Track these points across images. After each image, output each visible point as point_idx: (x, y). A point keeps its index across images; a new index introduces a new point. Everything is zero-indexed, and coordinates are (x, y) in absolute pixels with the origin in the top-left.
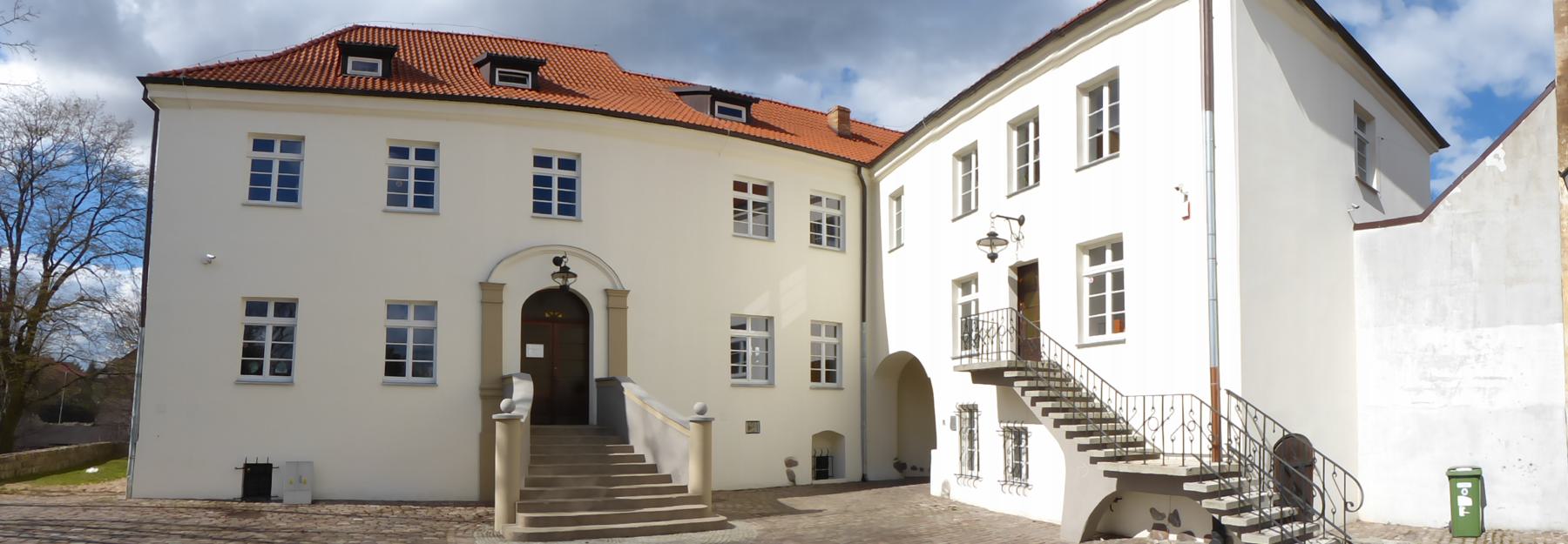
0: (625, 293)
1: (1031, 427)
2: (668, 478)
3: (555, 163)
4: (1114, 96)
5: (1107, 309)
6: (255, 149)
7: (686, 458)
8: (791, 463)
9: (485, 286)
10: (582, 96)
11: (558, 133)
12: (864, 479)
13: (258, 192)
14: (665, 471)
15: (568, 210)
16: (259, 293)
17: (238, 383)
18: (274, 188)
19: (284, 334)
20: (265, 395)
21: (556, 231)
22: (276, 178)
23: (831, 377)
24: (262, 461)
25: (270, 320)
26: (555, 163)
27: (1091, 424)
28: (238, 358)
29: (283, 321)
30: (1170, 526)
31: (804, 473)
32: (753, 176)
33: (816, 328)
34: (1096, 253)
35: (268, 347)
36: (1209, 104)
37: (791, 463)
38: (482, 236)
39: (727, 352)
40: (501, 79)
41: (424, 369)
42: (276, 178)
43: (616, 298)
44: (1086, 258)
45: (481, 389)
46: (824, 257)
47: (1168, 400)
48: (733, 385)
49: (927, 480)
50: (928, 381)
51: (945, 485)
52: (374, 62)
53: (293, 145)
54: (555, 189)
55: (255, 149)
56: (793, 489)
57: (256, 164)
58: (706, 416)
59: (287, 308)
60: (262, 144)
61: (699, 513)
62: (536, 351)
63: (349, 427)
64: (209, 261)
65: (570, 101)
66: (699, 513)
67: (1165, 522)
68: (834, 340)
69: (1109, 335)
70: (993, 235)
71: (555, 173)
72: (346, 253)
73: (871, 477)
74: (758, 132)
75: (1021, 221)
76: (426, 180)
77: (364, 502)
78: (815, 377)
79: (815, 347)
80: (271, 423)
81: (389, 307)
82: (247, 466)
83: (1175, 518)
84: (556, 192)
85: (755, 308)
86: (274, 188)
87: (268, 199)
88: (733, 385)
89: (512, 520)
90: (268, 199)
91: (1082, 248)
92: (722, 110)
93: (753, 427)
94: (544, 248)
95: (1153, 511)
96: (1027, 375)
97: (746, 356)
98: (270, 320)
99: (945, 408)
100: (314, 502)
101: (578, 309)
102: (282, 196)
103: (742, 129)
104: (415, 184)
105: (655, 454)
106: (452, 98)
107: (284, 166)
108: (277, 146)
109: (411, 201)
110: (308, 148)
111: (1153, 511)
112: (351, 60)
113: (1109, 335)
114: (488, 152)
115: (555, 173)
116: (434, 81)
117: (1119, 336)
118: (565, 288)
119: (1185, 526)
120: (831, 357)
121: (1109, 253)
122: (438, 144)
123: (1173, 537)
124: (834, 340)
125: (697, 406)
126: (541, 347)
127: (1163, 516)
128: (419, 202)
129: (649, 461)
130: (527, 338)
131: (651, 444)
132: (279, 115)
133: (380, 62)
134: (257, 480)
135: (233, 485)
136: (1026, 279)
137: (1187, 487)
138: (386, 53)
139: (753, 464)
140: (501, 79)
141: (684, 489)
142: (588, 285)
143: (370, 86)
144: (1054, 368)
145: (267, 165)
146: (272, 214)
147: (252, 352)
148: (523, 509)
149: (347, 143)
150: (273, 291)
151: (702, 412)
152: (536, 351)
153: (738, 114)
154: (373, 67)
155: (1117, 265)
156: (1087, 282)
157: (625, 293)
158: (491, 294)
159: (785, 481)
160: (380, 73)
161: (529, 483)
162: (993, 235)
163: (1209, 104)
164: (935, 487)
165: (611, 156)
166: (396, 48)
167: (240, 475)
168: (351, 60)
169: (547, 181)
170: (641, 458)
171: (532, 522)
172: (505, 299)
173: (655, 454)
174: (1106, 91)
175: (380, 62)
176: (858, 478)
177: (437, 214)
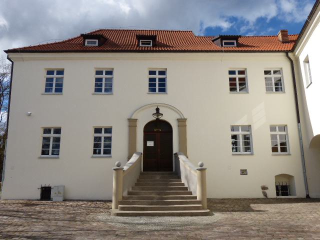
0: (185, 120)
3: (237, 73)
6: (47, 74)
8: (264, 188)
9: (130, 120)
10: (251, 46)
11: (157, 61)
12: (308, 196)
13: (48, 89)
15: (163, 89)
16: (48, 126)
17: (92, 157)
18: (157, 88)
19: (57, 140)
20: (49, 162)
21: (158, 98)
22: (54, 84)
23: (284, 149)
24: (47, 186)
25: (103, 135)
26: (237, 73)
28: (40, 149)
29: (108, 135)
31: (272, 193)
32: (237, 67)
33: (273, 128)
35: (51, 144)
37: (264, 188)
38: (130, 100)
39: (231, 140)
40: (142, 44)
41: (108, 152)
42: (103, 84)
43: (182, 122)
48: (233, 155)
52: (101, 41)
53: (61, 72)
54: (157, 82)
55: (47, 74)
56: (266, 200)
57: (48, 80)
58: (204, 167)
59: (58, 131)
60: (50, 72)
61: (198, 208)
62: (150, 144)
63: (82, 172)
64: (30, 115)
65: (250, 49)
66: (198, 208)
68: (284, 133)
71: (237, 76)
72: (80, 109)
73: (312, 195)
74: (240, 49)
76: (163, 82)
77: (79, 200)
78: (275, 149)
79: (273, 137)
80: (51, 172)
82: (42, 188)
84: (158, 83)
85: (242, 121)
86: (157, 88)
87: (101, 91)
89: (117, 208)
90: (101, 91)
92: (226, 44)
93: (244, 172)
94: (151, 105)
97: (242, 142)
98: (103, 135)
100: (65, 200)
101: (167, 127)
102: (57, 91)
103: (237, 49)
104: (103, 84)
106: (259, 51)
107: (160, 80)
108: (55, 73)
109: (157, 90)
110: (114, 73)
112: (86, 40)
114: (131, 70)
115: (157, 76)
116: (167, 46)
118: (158, 120)
120: (284, 141)
122: (166, 69)
124: (284, 133)
125: (200, 163)
126: (153, 142)
128: (160, 90)
129: (186, 186)
130: (146, 139)
131: (186, 177)
132: (55, 61)
133: (97, 41)
134: (46, 193)
135: (37, 194)
138: (153, 38)
139: (249, 188)
140: (142, 44)
141: (196, 198)
142: (169, 116)
143: (146, 49)
145: (154, 80)
146: (53, 97)
147: (45, 146)
149: (80, 70)
150: (103, 124)
151: (201, 166)
152: (150, 144)
153: (233, 44)
154: (95, 43)
157: (185, 120)
158: (132, 123)
159: (261, 196)
160: (97, 45)
161: (129, 193)
165: (173, 64)
166: (156, 36)
167: (40, 190)
168: (86, 40)
169: (234, 79)
172: (187, 124)
175: (97, 41)
176: (304, 195)
177: (167, 94)
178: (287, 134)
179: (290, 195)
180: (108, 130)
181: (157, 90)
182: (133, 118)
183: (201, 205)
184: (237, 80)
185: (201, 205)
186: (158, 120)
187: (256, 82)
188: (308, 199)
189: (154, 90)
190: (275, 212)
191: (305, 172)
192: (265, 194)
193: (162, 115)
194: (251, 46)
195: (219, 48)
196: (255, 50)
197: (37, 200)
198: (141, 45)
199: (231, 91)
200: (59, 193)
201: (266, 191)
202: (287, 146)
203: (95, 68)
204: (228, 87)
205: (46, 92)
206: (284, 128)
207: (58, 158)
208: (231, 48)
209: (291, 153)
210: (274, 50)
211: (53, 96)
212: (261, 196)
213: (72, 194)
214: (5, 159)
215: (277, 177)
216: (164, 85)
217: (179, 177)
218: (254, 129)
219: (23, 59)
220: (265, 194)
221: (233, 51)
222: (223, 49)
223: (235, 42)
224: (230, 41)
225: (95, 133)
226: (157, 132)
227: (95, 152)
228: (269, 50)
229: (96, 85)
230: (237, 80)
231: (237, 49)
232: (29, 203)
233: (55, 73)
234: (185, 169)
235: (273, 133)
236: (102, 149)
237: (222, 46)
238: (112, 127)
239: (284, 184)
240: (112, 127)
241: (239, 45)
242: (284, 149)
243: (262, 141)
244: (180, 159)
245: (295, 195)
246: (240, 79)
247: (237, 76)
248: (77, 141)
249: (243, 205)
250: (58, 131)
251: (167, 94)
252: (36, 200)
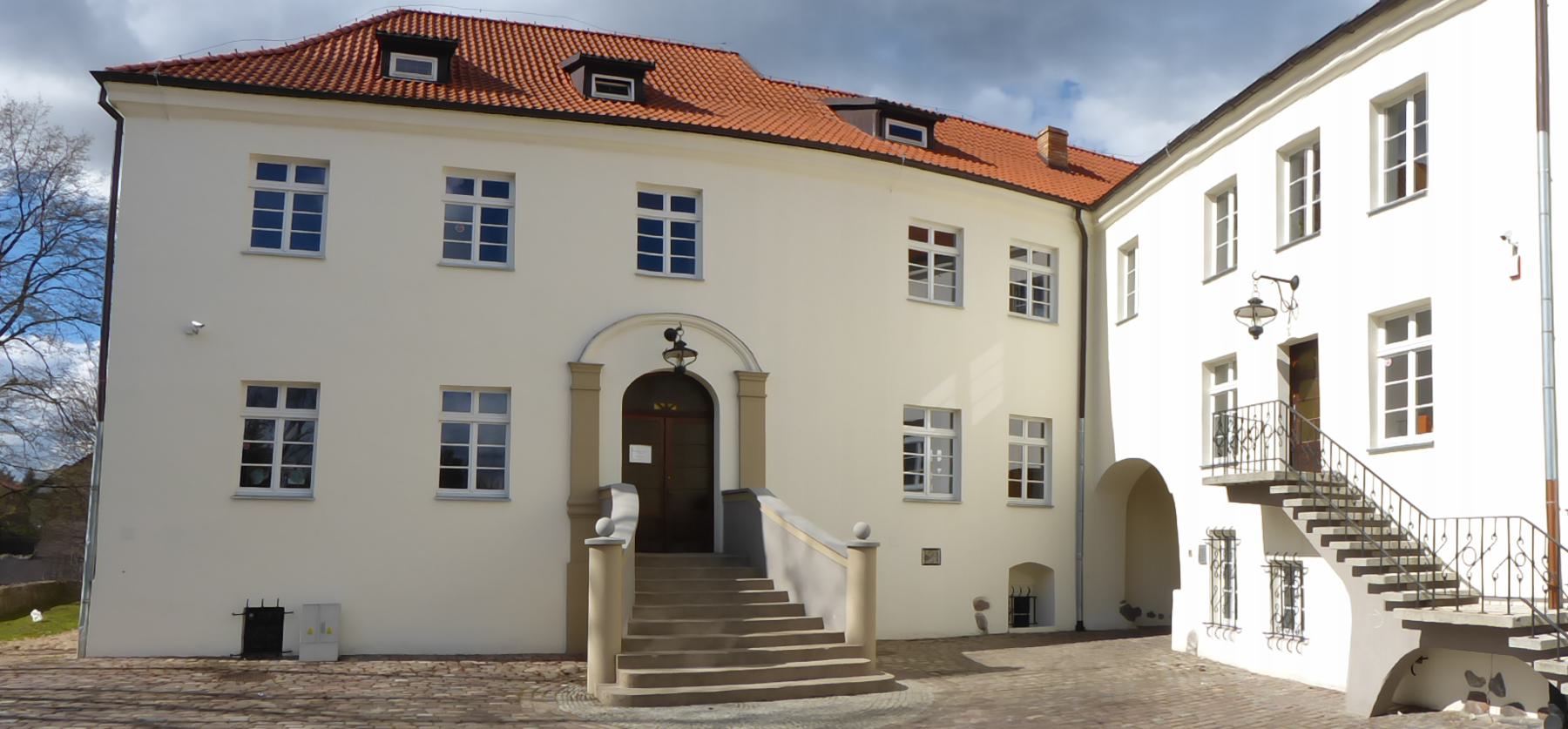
0: (762, 377)
1: (1307, 561)
2: (819, 623)
4: (1421, 114)
5: (1409, 401)
7: (841, 591)
8: (981, 605)
10: (704, 112)
11: (671, 162)
12: (1080, 626)
14: (813, 613)
15: (685, 264)
17: (237, 498)
20: (274, 515)
21: (668, 294)
22: (289, 216)
23: (1035, 491)
24: (270, 603)
25: (282, 413)
26: (667, 203)
27: (1387, 557)
30: (1491, 696)
31: (998, 617)
32: (937, 219)
33: (1015, 426)
34: (1394, 325)
35: (277, 447)
36: (1543, 122)
37: (981, 605)
39: (899, 455)
40: (401, 65)
41: (493, 477)
42: (289, 216)
43: (750, 383)
44: (1382, 333)
45: (570, 505)
46: (1030, 329)
47: (1439, 524)
48: (906, 500)
49: (1166, 630)
50: (1169, 499)
51: (1192, 637)
53: (313, 172)
63: (385, 553)
64: (196, 331)
67: (1485, 689)
68: (1040, 442)
69: (1412, 437)
70: (1256, 303)
71: (667, 216)
72: (386, 320)
73: (1088, 625)
74: (936, 159)
75: (1295, 283)
79: (1015, 451)
81: (1011, 421)
82: (248, 611)
83: (1498, 685)
85: (938, 397)
88: (906, 500)
89: (610, 678)
91: (1377, 319)
93: (931, 557)
95: (1469, 675)
96: (1303, 493)
98: (282, 413)
99: (1191, 533)
100: (342, 658)
101: (700, 397)
103: (921, 156)
105: (799, 589)
109: (667, 264)
111: (1469, 675)
112: (394, 57)
113: (1412, 437)
114: (572, 188)
116: (509, 89)
117: (1425, 438)
119: (1512, 693)
120: (1037, 465)
121: (1412, 326)
122: (513, 176)
123: (1495, 710)
124: (1040, 442)
125: (858, 527)
127: (1481, 681)
128: (678, 266)
130: (631, 435)
131: (791, 574)
132: (295, 130)
133: (434, 61)
134: (263, 630)
135: (231, 637)
136: (1301, 362)
137: (1515, 642)
139: (934, 605)
141: (840, 637)
142: (712, 366)
144: (1337, 481)
146: (284, 269)
148: (625, 663)
149: (390, 170)
150: (284, 372)
152: (642, 454)
153: (916, 136)
154: (426, 68)
155: (1424, 341)
156: (1382, 365)
157: (762, 377)
158: (583, 378)
162: (1256, 303)
163: (1543, 122)
164: (1178, 640)
166: (457, 43)
168: (394, 57)
169: (656, 226)
170: (784, 596)
171: (638, 681)
173: (799, 589)
174: (1410, 107)
175: (434, 61)
177: (701, 280)
178: (1050, 446)
179: (1035, 624)
180: (498, 399)
181: (667, 264)
182: (587, 359)
183: (965, 653)
184: (667, 229)
185: (965, 653)
186: (680, 370)
187: (986, 274)
188: (1080, 633)
189: (656, 265)
190: (1036, 667)
191: (1079, 559)
192: (982, 623)
193: (695, 354)
194: (704, 112)
195: (870, 141)
196: (918, 159)
197: (231, 657)
198: (392, 71)
199: (640, 266)
200: (323, 630)
201: (985, 613)
202: (1045, 482)
203: (446, 168)
204: (633, 252)
205: (253, 244)
206: (1042, 427)
207: (310, 498)
208: (902, 149)
209: (1053, 503)
210: (864, 148)
211: (284, 261)
212: (972, 629)
213: (365, 636)
214: (96, 500)
215: (1017, 571)
216: (501, 235)
217: (761, 571)
218: (968, 423)
219: (165, 112)
220: (982, 623)
221: (911, 163)
222: (884, 147)
223: (924, 130)
224: (908, 131)
225: (445, 409)
226: (665, 413)
227: (247, 479)
228: (815, 139)
229: (259, 219)
230: (667, 229)
231: (929, 158)
232: (212, 666)
233: (291, 174)
234: (785, 537)
235: (1016, 440)
236: (473, 468)
237: (881, 134)
238: (318, 384)
239: (1024, 594)
240: (318, 384)
241: (934, 146)
242: (1035, 491)
243: (986, 462)
244: (763, 510)
245: (1050, 623)
246: (677, 228)
247: (667, 216)
248: (376, 444)
249: (940, 655)
250: (304, 396)
251: (701, 280)
252: (390, 657)
